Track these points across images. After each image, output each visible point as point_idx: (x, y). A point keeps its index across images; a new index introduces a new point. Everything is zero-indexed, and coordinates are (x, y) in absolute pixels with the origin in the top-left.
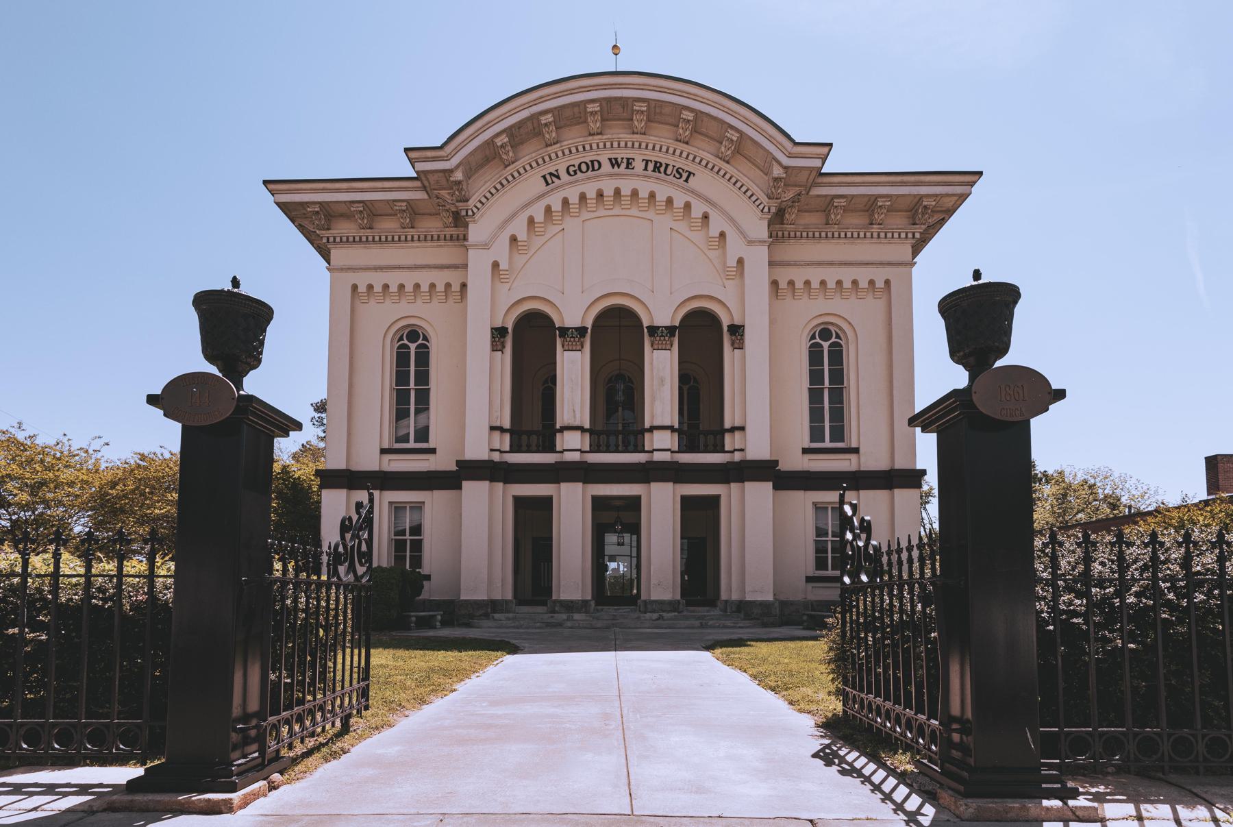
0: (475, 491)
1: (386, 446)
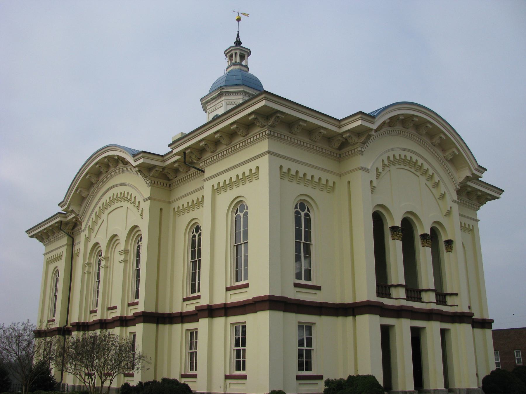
0: (202, 325)
1: (185, 297)
